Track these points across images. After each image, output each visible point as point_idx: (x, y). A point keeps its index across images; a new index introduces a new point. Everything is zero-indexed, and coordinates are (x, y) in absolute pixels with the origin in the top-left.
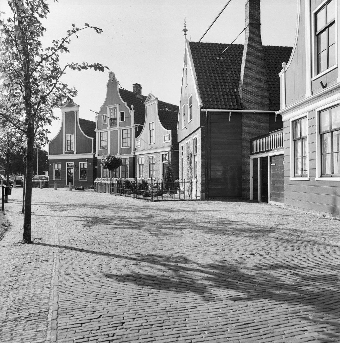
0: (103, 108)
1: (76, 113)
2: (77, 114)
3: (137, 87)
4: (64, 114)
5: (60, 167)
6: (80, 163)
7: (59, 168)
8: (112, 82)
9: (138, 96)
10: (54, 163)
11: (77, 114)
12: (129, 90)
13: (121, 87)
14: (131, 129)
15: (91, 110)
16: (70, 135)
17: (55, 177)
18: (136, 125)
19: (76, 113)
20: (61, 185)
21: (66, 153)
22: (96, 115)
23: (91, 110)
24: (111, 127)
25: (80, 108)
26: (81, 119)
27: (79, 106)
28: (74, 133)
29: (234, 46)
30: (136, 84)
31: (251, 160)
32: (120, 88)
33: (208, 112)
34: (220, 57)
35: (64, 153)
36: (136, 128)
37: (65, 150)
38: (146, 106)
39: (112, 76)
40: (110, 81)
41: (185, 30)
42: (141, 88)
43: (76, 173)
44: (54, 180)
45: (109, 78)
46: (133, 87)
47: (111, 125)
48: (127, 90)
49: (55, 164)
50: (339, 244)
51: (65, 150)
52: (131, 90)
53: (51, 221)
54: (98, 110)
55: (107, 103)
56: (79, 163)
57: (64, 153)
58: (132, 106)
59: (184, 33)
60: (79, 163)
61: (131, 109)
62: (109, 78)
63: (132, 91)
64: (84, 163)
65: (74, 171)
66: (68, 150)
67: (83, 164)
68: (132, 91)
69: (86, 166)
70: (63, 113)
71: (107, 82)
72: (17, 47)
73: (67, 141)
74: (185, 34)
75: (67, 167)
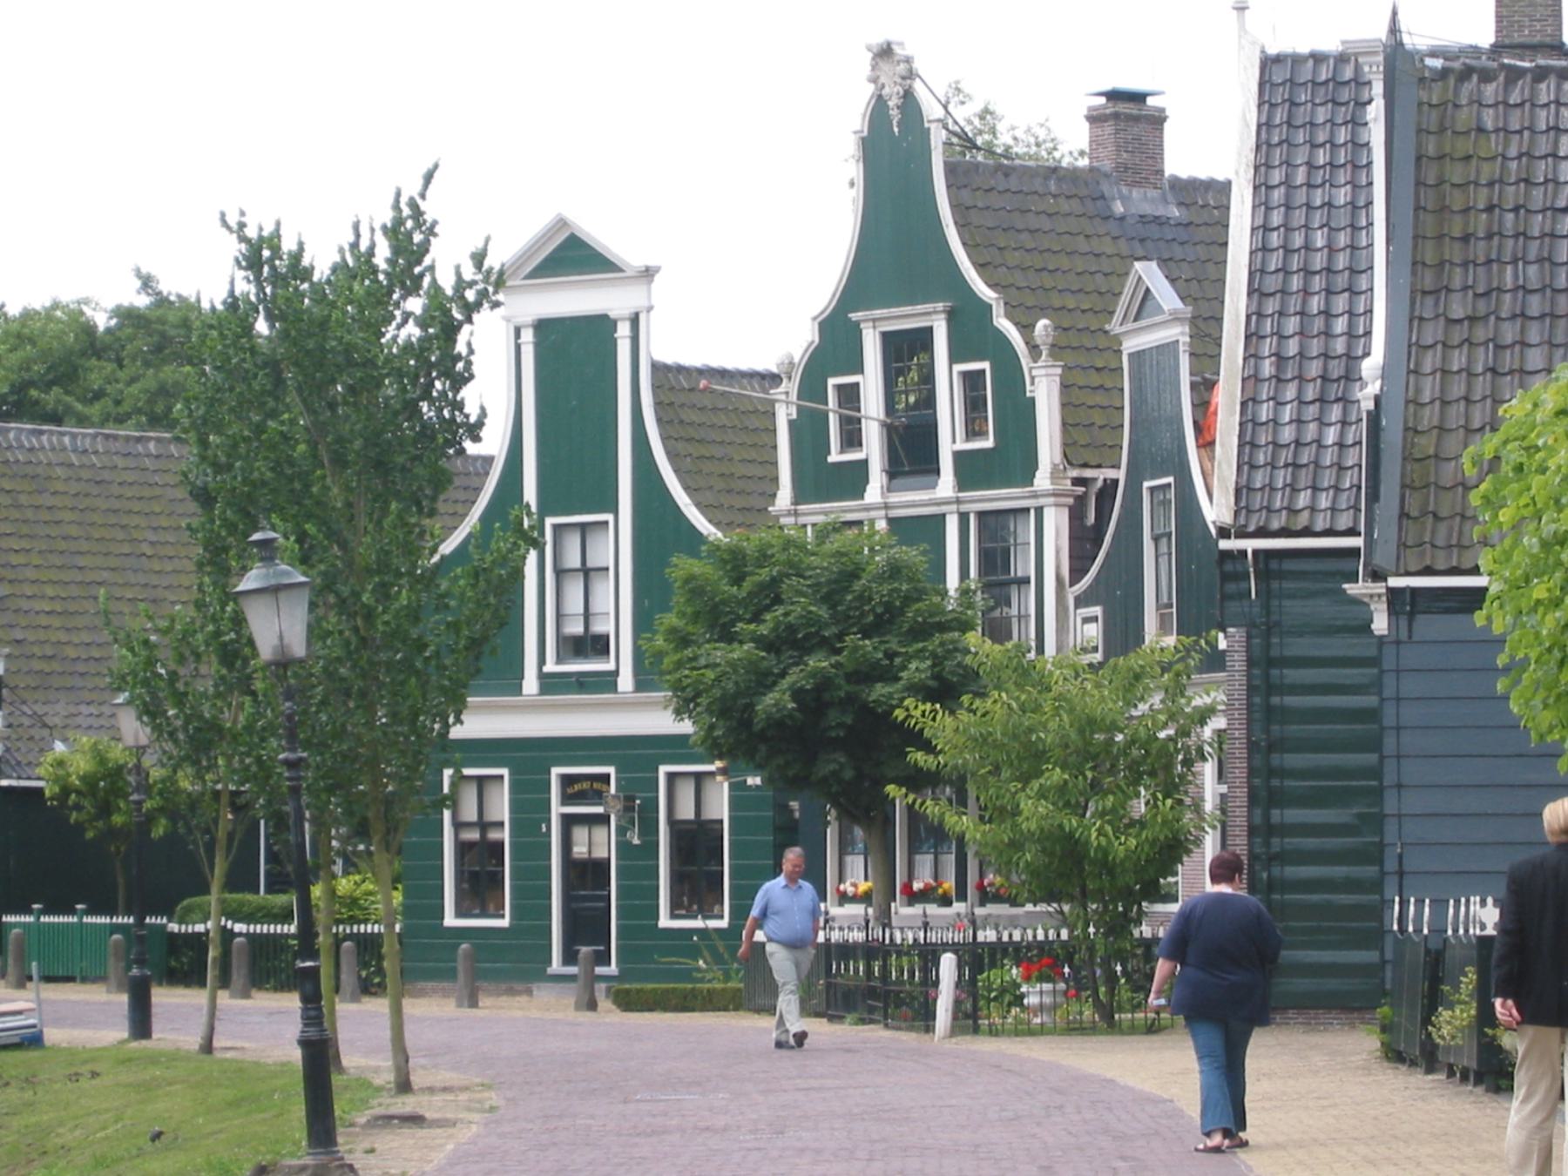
4: (528, 336)
5: (501, 806)
6: (671, 777)
8: (895, 114)
14: (1039, 511)
16: (584, 528)
18: (1078, 481)
19: (623, 330)
20: (509, 963)
24: (897, 482)
28: (614, 509)
30: (1114, 96)
33: (1255, 552)
35: (530, 684)
36: (1081, 500)
37: (542, 661)
38: (1130, 345)
40: (879, 106)
42: (1158, 120)
43: (638, 859)
44: (450, 920)
45: (872, 87)
46: (1094, 118)
50: (5, 692)
51: (542, 661)
52: (1072, 142)
55: (866, 282)
56: (663, 769)
57: (530, 684)
60: (663, 769)
61: (1034, 350)
62: (872, 87)
64: (699, 778)
65: (624, 848)
66: (580, 833)
69: (720, 805)
73: (560, 616)
75: (557, 809)
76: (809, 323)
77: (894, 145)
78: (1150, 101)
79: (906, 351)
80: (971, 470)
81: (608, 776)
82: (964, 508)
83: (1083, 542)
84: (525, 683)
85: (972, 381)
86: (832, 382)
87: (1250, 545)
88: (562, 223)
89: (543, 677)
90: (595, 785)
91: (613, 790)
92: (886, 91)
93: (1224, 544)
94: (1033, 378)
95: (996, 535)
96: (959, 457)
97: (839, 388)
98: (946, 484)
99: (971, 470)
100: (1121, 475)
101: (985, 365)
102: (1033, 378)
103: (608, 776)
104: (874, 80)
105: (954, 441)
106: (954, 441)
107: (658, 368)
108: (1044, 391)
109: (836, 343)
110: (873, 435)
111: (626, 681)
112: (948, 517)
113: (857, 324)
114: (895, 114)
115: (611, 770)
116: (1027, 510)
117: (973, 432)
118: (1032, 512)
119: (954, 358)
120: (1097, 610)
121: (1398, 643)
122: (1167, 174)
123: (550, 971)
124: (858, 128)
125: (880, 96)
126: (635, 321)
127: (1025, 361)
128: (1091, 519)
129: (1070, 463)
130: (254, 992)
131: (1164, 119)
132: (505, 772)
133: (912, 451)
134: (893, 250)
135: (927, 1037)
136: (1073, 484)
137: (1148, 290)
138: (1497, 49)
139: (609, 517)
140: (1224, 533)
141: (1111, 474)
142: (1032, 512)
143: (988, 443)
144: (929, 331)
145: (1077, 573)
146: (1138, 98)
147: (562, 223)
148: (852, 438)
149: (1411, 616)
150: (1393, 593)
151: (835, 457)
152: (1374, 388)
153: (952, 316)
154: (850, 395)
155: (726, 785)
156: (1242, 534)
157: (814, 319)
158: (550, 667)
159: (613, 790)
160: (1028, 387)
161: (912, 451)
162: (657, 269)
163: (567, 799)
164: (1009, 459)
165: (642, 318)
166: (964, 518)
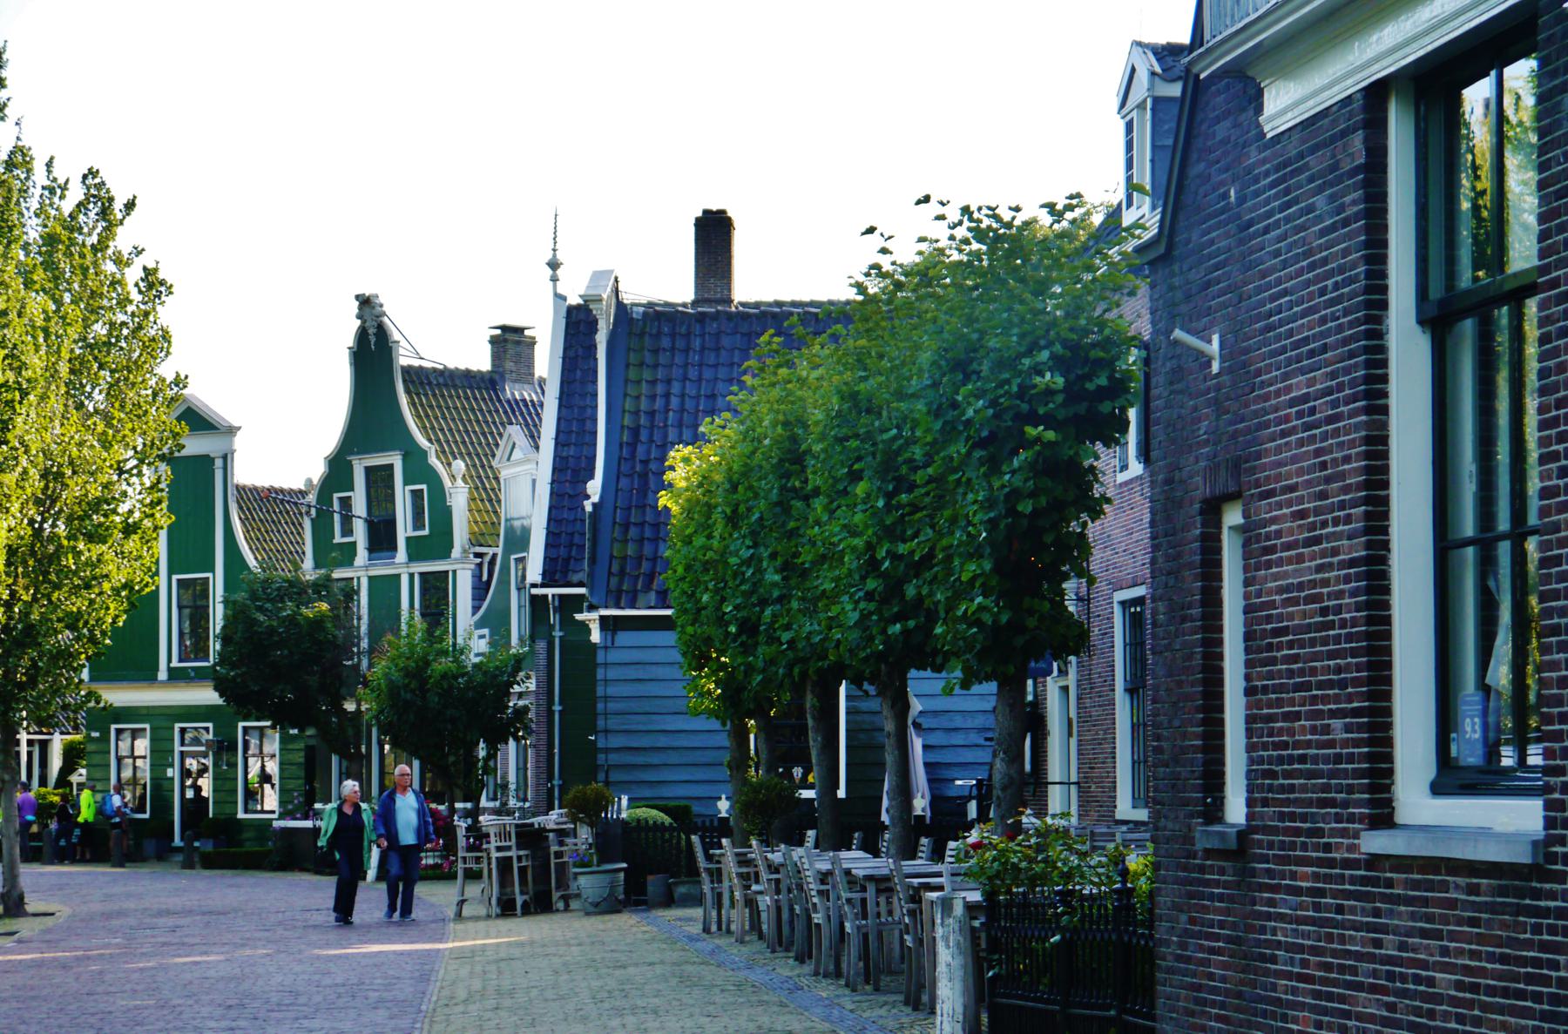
6: (245, 729)
8: (373, 339)
9: (512, 391)
10: (113, 727)
12: (462, 367)
17: (391, 476)
18: (477, 555)
19: (219, 463)
21: (176, 676)
25: (239, 442)
26: (255, 490)
27: (232, 431)
30: (504, 328)
31: (1225, 531)
35: (163, 675)
36: (480, 565)
37: (170, 660)
40: (362, 335)
41: (554, 265)
45: (359, 322)
46: (494, 341)
47: (372, 549)
48: (451, 366)
51: (170, 660)
52: (481, 361)
53: (1196, 468)
57: (163, 675)
58: (459, 465)
59: (550, 272)
62: (359, 322)
64: (261, 729)
67: (256, 734)
71: (349, 340)
74: (554, 279)
77: (372, 350)
78: (527, 332)
79: (379, 480)
80: (418, 549)
82: (412, 570)
83: (480, 589)
85: (417, 495)
86: (336, 495)
89: (170, 670)
93: (535, 591)
95: (435, 590)
96: (408, 539)
97: (340, 499)
98: (402, 554)
99: (418, 549)
100: (499, 551)
101: (424, 487)
108: (459, 498)
109: (338, 470)
110: (360, 528)
112: (538, 579)
114: (373, 339)
117: (415, 528)
119: (406, 483)
120: (486, 631)
121: (606, 648)
126: (225, 457)
127: (447, 483)
128: (485, 578)
132: (147, 726)
133: (382, 538)
134: (372, 415)
135: (1426, 788)
138: (695, 303)
139: (210, 575)
140: (534, 586)
141: (494, 550)
143: (426, 532)
144: (391, 466)
145: (476, 609)
146: (519, 331)
148: (347, 530)
149: (614, 632)
150: (602, 617)
151: (338, 539)
152: (595, 498)
154: (346, 503)
156: (543, 585)
158: (175, 664)
161: (382, 538)
163: (144, 672)
164: (435, 543)
166: (411, 576)
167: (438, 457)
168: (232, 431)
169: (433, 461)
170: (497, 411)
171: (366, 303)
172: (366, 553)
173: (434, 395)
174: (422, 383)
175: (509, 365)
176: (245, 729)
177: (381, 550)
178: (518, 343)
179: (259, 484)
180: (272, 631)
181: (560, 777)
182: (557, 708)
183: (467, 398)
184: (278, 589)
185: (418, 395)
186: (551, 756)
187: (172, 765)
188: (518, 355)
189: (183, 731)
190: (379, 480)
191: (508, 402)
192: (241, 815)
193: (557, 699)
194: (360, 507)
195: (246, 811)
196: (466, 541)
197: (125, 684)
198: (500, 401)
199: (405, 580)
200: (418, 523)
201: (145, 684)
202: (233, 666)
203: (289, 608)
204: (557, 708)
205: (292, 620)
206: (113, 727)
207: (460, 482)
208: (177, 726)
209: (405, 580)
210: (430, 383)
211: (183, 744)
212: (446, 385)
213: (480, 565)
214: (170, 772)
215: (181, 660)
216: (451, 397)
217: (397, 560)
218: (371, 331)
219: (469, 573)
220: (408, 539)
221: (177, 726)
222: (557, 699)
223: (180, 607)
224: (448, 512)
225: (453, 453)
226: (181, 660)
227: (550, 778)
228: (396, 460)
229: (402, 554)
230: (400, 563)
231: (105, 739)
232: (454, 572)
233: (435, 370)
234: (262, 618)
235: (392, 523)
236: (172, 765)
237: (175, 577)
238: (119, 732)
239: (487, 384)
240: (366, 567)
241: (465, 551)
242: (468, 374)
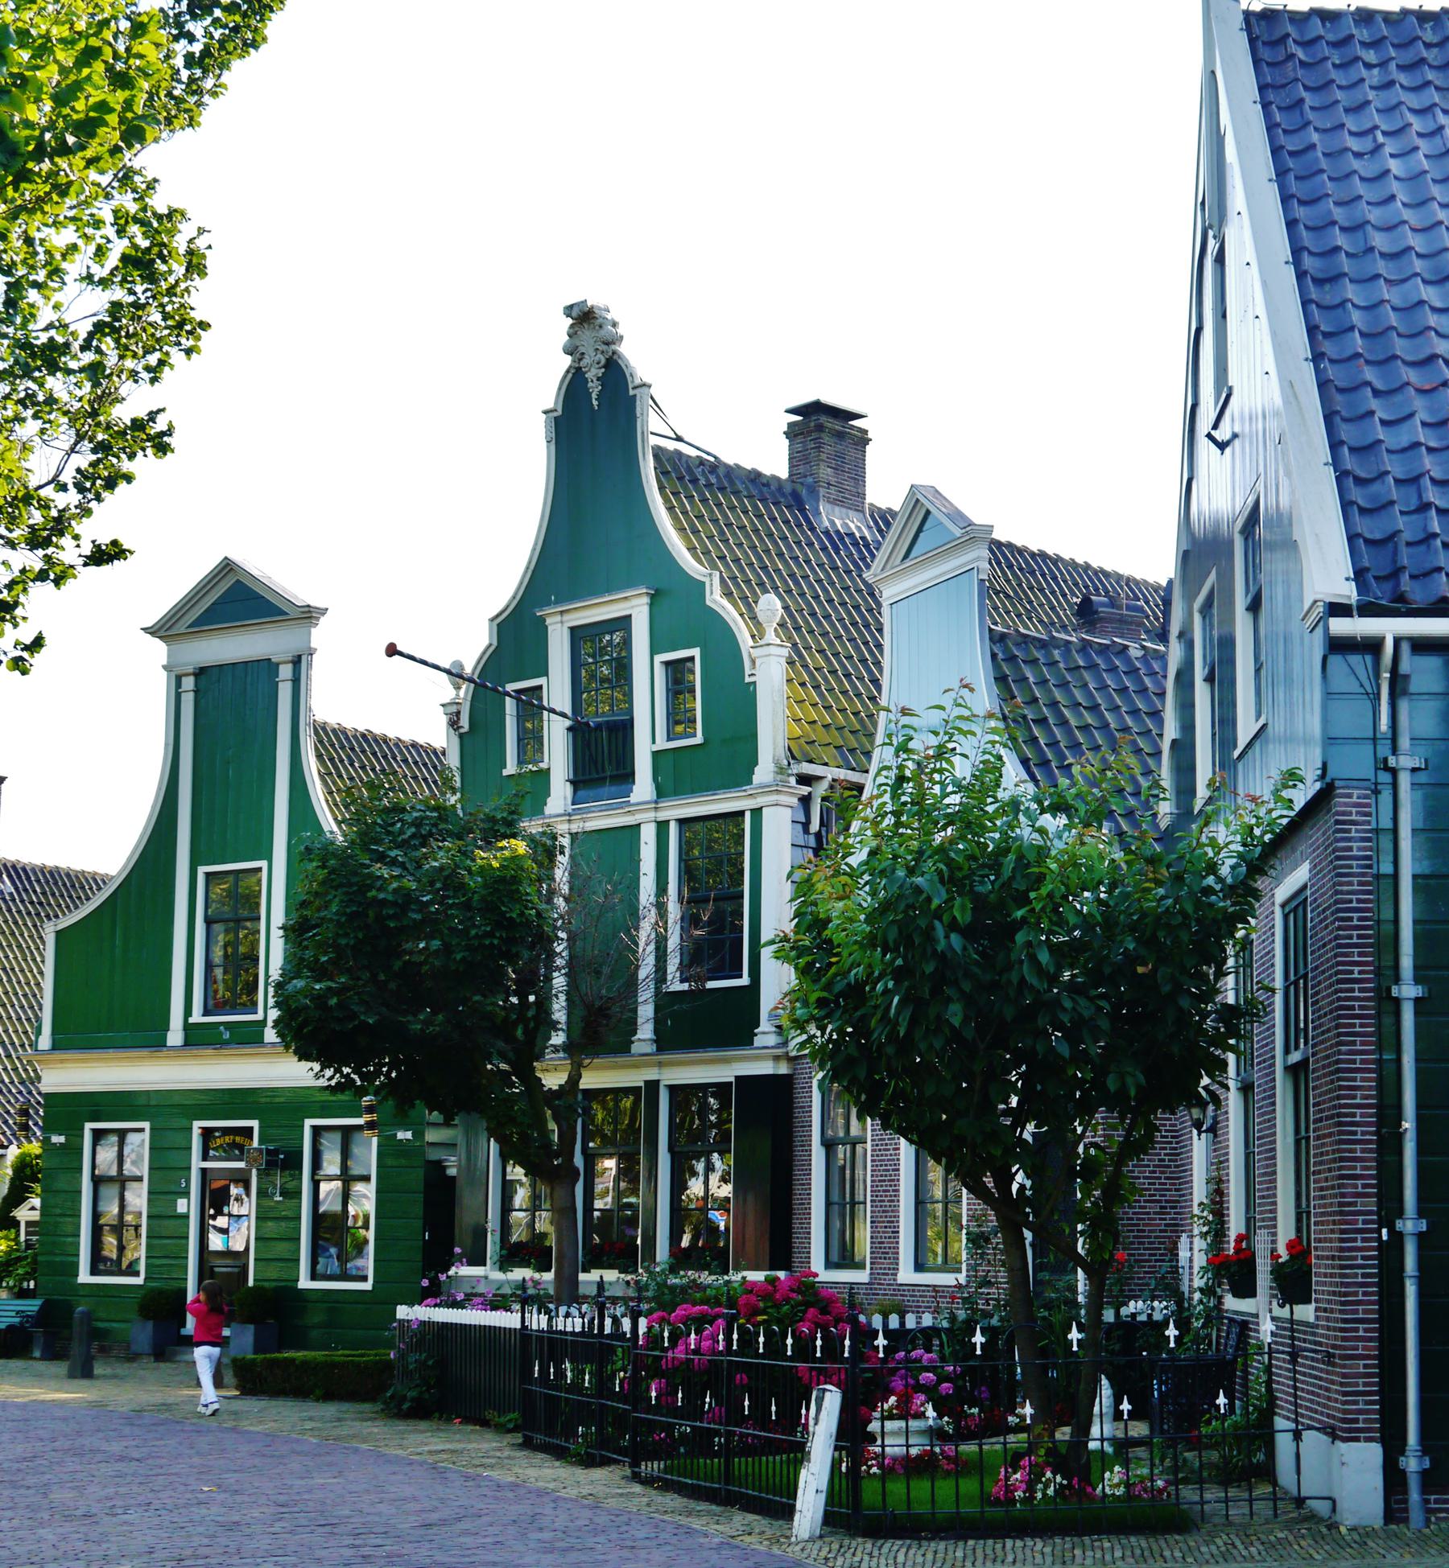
0: (517, 636)
1: (286, 671)
2: (296, 681)
3: (825, 430)
4: (189, 683)
6: (317, 1131)
7: (129, 1169)
8: (595, 389)
9: (832, 517)
10: (89, 1126)
11: (296, 681)
12: (748, 465)
13: (679, 439)
15: (392, 650)
18: (805, 780)
19: (286, 671)
21: (196, 1037)
22: (445, 691)
23: (392, 650)
25: (319, 636)
26: (340, 732)
27: (309, 615)
29: (577, 1445)
32: (672, 445)
34: (492, 944)
35: (175, 1037)
37: (188, 1011)
39: (587, 336)
40: (574, 386)
42: (863, 440)
46: (792, 432)
48: (729, 459)
49: (98, 1135)
51: (188, 1011)
52: (772, 458)
54: (470, 644)
55: (559, 567)
56: (309, 1123)
57: (175, 1037)
58: (770, 606)
60: (309, 1123)
61: (758, 633)
63: (783, 473)
64: (347, 1132)
67: (337, 1137)
68: (783, 473)
70: (179, 679)
71: (548, 394)
72: (1374, 66)
76: (487, 624)
77: (596, 410)
80: (674, 776)
81: (251, 1129)
82: (662, 816)
84: (170, 1035)
85: (677, 672)
87: (1388, 628)
88: (227, 567)
89: (188, 1028)
90: (238, 1139)
91: (255, 1144)
92: (586, 361)
93: (1340, 626)
94: (753, 662)
98: (643, 786)
99: (674, 776)
102: (753, 662)
103: (251, 1129)
104: (569, 351)
105: (654, 742)
106: (654, 742)
107: (322, 731)
108: (769, 670)
111: (270, 1035)
113: (542, 619)
114: (595, 389)
115: (254, 1124)
116: (742, 813)
118: (748, 815)
119: (654, 650)
122: (869, 500)
123: (183, 1332)
124: (550, 405)
125: (579, 369)
126: (297, 662)
129: (794, 757)
130: (1419, 794)
131: (867, 441)
133: (602, 758)
136: (798, 782)
137: (928, 512)
139: (263, 864)
140: (1337, 609)
142: (748, 815)
147: (227, 567)
148: (531, 741)
151: (511, 768)
153: (655, 598)
155: (375, 1140)
156: (1368, 610)
157: (492, 620)
158: (197, 1017)
159: (255, 1144)
160: (747, 671)
161: (602, 758)
162: (323, 611)
164: (726, 754)
165: (304, 658)
166: (662, 827)
167: (728, 594)
168: (309, 615)
169: (716, 598)
170: (810, 544)
171: (584, 317)
172: (569, 788)
173: (704, 501)
174: (681, 478)
175: (825, 472)
176: (317, 1131)
177: (600, 781)
178: (840, 435)
179: (348, 724)
180: (406, 900)
181: (1421, 1213)
182: (1408, 990)
183: (760, 516)
184: (418, 823)
185: (676, 494)
186: (1389, 1143)
187: (186, 1194)
188: (840, 456)
189: (207, 1133)
190: (602, 650)
191: (827, 533)
192: (305, 1283)
193: (1407, 962)
194: (557, 689)
195: (314, 1276)
196: (782, 753)
197: (111, 1053)
198: (812, 529)
199: (648, 834)
200: (678, 718)
201: (145, 1052)
202: (320, 973)
203: (441, 856)
204: (1408, 990)
205: (449, 880)
206: (89, 1126)
207: (771, 636)
208: (197, 1125)
209: (648, 834)
210: (695, 481)
211: (205, 1158)
212: (722, 489)
213: (805, 801)
214: (182, 1206)
215: (206, 1013)
216: (732, 508)
217: (633, 798)
218: (593, 373)
219: (787, 814)
220: (656, 755)
221: (197, 1125)
222: (1407, 962)
223: (209, 922)
224: (747, 697)
225: (761, 584)
226: (207, 1012)
227: (1390, 1209)
228: (638, 609)
229: (643, 786)
230: (643, 806)
231: (73, 1150)
232: (757, 812)
233: (702, 462)
234: (385, 873)
235: (624, 729)
236: (186, 1194)
237: (202, 870)
238: (98, 1135)
239: (789, 498)
240: (569, 816)
241: (781, 770)
242: (755, 477)
